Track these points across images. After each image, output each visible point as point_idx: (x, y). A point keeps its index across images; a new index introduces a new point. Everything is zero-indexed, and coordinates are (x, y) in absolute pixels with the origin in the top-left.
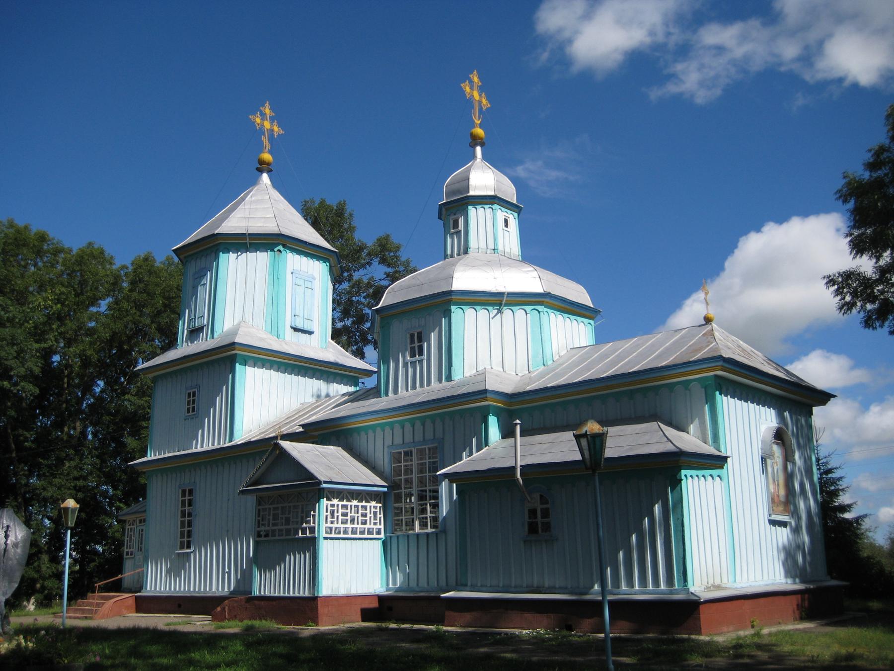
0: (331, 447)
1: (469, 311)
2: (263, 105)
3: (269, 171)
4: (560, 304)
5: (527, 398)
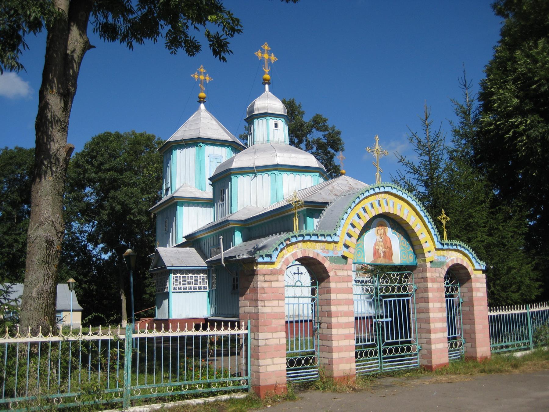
0: (188, 248)
1: (240, 178)
2: (199, 67)
3: (269, 84)
4: (289, 168)
5: (250, 222)
